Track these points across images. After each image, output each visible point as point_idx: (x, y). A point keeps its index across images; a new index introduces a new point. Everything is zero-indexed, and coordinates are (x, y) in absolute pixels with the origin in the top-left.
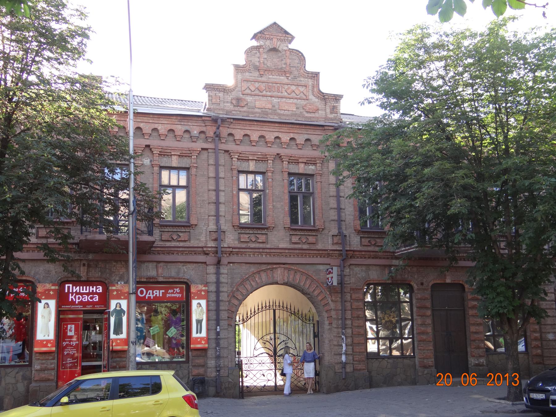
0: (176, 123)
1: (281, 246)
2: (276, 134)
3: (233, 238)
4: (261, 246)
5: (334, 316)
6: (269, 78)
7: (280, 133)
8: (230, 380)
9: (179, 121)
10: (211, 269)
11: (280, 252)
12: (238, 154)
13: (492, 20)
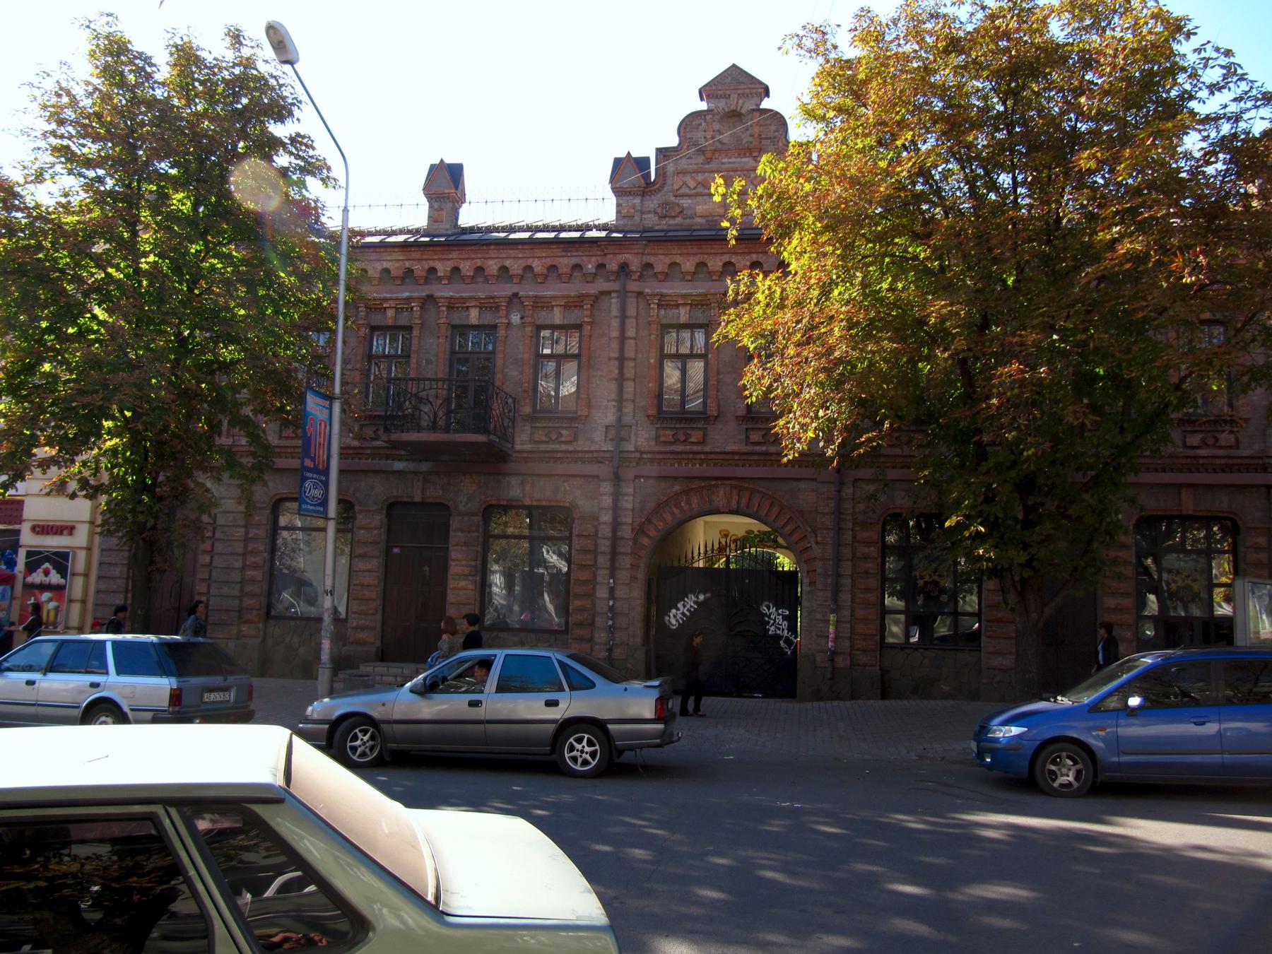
0: (560, 254)
1: (729, 448)
3: (647, 436)
4: (695, 448)
5: (819, 570)
6: (722, 163)
8: (629, 666)
10: (606, 488)
11: (727, 458)
13: (1053, 3)
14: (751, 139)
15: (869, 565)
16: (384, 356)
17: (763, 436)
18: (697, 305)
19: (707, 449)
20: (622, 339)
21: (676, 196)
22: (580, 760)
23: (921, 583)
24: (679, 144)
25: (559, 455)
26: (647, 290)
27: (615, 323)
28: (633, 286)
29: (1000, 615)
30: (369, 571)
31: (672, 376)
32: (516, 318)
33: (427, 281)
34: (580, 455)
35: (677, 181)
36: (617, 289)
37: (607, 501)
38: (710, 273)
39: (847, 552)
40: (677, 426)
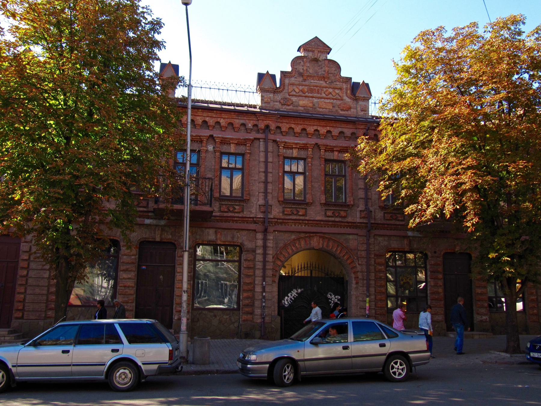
2: (315, 128)
3: (278, 211)
4: (301, 218)
6: (311, 82)
7: (319, 127)
10: (260, 236)
11: (317, 223)
12: (284, 143)
14: (324, 73)
15: (381, 275)
16: (228, 168)
17: (333, 213)
18: (301, 149)
19: (307, 218)
20: (266, 162)
21: (289, 95)
22: (397, 373)
23: (402, 282)
24: (292, 71)
25: (236, 219)
26: (278, 140)
27: (262, 154)
28: (271, 137)
29: (436, 297)
30: (129, 279)
31: (288, 183)
32: (210, 148)
33: (325, 137)
34: (246, 219)
35: (291, 88)
36: (264, 137)
37: (260, 243)
38: (307, 134)
39: (372, 268)
40: (293, 206)
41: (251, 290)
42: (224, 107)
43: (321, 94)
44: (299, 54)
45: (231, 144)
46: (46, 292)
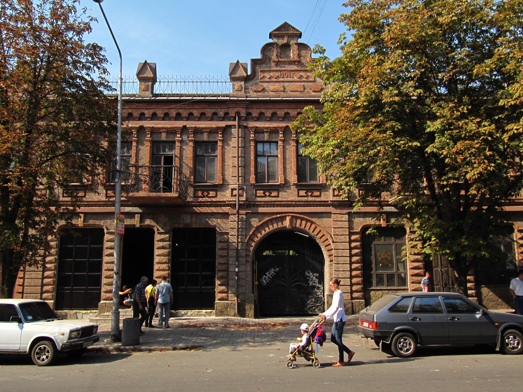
0: (206, 107)
7: (289, 110)
9: (208, 106)
12: (255, 128)
19: (279, 199)
41: (225, 271)
42: (194, 98)
43: (293, 78)
44: (271, 41)
45: (204, 133)
46: (41, 276)
